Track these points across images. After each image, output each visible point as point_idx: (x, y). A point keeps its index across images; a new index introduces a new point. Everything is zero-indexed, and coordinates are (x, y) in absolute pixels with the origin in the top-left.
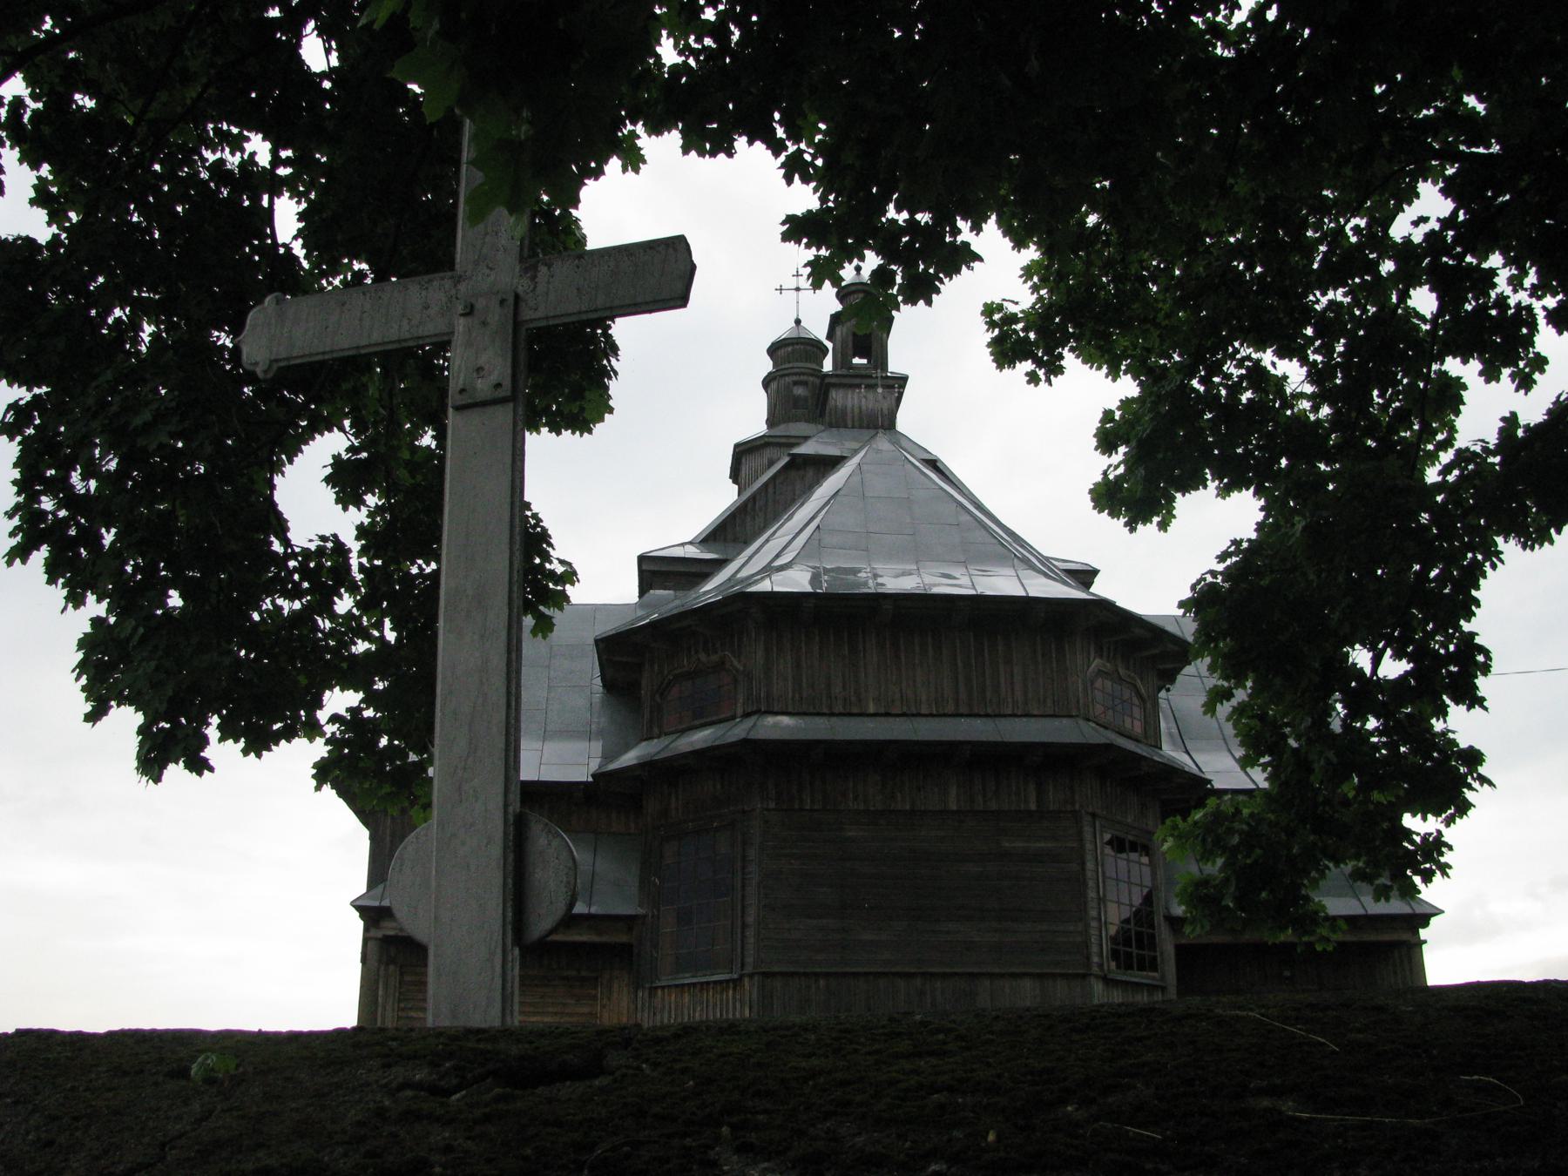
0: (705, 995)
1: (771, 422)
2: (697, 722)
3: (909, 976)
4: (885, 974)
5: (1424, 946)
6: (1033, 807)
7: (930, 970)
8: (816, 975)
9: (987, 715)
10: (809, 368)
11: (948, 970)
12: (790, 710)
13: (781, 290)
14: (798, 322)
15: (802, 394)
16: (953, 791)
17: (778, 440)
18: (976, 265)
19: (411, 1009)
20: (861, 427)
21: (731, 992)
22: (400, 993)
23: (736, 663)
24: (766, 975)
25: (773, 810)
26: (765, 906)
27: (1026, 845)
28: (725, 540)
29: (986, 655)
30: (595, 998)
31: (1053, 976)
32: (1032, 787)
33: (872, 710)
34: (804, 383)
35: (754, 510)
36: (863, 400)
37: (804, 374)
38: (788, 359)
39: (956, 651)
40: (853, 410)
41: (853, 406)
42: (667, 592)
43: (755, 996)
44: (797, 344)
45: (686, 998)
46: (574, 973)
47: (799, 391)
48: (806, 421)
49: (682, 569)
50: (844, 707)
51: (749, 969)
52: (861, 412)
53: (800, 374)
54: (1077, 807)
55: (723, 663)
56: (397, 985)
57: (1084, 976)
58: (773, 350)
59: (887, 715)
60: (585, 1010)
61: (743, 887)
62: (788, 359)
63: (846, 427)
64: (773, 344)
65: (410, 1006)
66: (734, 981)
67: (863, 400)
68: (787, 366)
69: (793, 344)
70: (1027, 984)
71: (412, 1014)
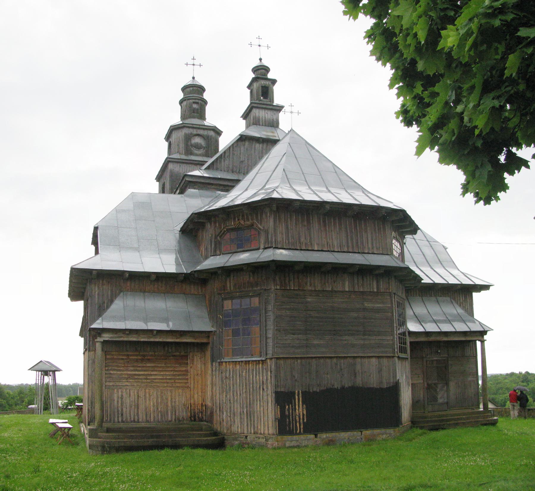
0: (248, 366)
1: (183, 117)
2: (239, 250)
3: (331, 358)
4: (323, 357)
5: (485, 342)
6: (375, 290)
7: (339, 355)
8: (297, 358)
9: (359, 253)
10: (199, 97)
11: (346, 355)
12: (285, 247)
13: (187, 64)
14: (194, 78)
15: (196, 107)
16: (347, 284)
17: (188, 125)
18: (383, 67)
19: (111, 370)
20: (265, 126)
21: (261, 365)
22: (105, 363)
23: (259, 226)
24: (277, 358)
25: (279, 289)
26: (276, 330)
27: (373, 305)
28: (213, 169)
29: (358, 228)
30: (187, 364)
31: (383, 357)
32: (375, 283)
33: (316, 249)
34: (197, 103)
35: (224, 157)
36: (266, 115)
37: (197, 99)
38: (190, 93)
39: (347, 226)
40: (262, 118)
41: (262, 116)
42: (195, 190)
43: (273, 367)
44: (195, 87)
45: (238, 367)
46: (178, 354)
47: (195, 106)
48: (197, 118)
49: (203, 181)
50: (306, 247)
51: (269, 356)
52: (265, 119)
53: (195, 99)
54: (391, 291)
55: (253, 225)
56: (104, 360)
57: (393, 357)
58: (184, 89)
59: (322, 251)
60: (184, 369)
61: (266, 321)
62: (190, 93)
63: (260, 125)
64: (184, 86)
65: (110, 369)
66: (262, 361)
67: (266, 115)
68: (192, 95)
69: (193, 87)
70: (374, 360)
71: (112, 372)
